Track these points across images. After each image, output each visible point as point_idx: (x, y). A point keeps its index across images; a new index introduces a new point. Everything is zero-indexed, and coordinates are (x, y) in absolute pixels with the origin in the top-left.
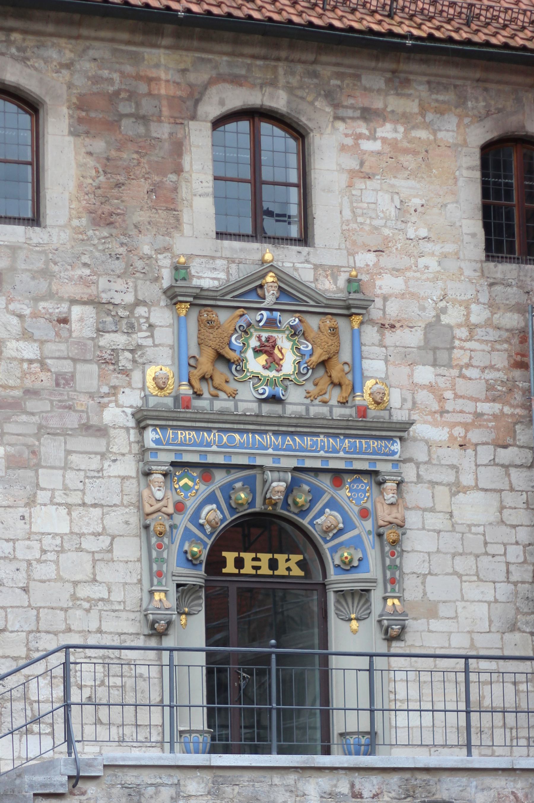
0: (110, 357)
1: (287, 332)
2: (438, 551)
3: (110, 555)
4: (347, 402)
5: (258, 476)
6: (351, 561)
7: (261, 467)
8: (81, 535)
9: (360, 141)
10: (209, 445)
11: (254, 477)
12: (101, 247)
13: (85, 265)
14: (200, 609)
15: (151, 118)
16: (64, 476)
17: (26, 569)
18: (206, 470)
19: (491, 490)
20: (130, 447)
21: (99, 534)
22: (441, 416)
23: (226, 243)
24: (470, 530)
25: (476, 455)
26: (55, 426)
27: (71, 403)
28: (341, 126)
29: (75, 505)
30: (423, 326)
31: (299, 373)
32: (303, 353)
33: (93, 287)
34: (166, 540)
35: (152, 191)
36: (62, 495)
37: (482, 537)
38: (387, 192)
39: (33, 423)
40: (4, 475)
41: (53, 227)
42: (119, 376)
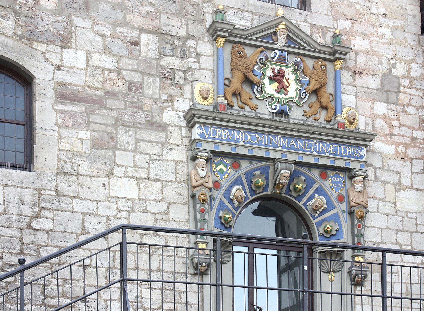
0: (168, 74)
1: (292, 68)
2: (387, 228)
3: (167, 216)
4: (331, 121)
5: (271, 166)
6: (331, 231)
7: (273, 159)
8: (147, 201)
11: (268, 167)
14: (229, 259)
16: (134, 157)
17: (105, 222)
18: (236, 158)
20: (182, 140)
21: (160, 201)
22: (391, 138)
24: (407, 216)
26: (128, 120)
27: (140, 104)
29: (142, 179)
30: (381, 75)
31: (300, 98)
32: (302, 83)
33: (157, 21)
34: (207, 206)
36: (133, 170)
37: (414, 220)
39: (112, 116)
40: (90, 152)
42: (175, 88)
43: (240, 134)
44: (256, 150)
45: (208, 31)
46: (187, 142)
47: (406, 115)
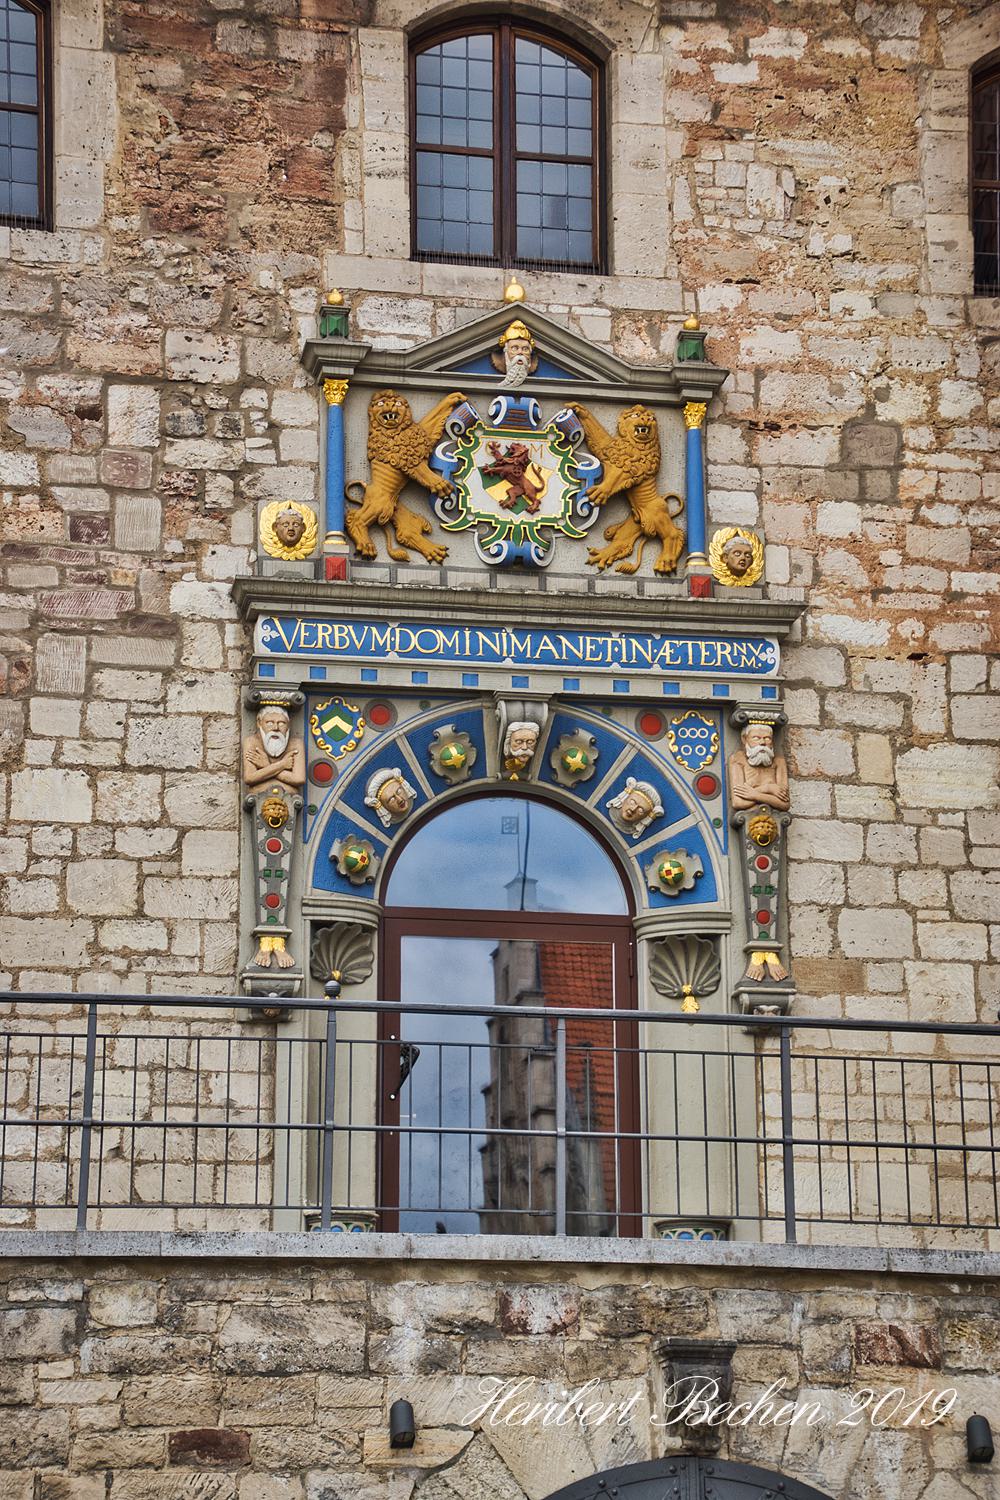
0: (186, 485)
2: (865, 861)
4: (674, 571)
6: (679, 879)
8: (115, 827)
9: (713, 66)
10: (381, 651)
11: (478, 715)
12: (170, 273)
13: (138, 306)
14: (367, 972)
15: (279, 21)
16: (83, 713)
18: (379, 701)
19: (980, 742)
20: (225, 657)
21: (154, 825)
22: (874, 599)
23: (431, 268)
25: (948, 674)
27: (102, 572)
28: (674, 36)
29: (106, 769)
31: (574, 517)
34: (287, 835)
35: (279, 165)
37: (961, 835)
38: (769, 164)
41: (70, 230)
42: (206, 521)
43: (388, 633)
44: (437, 673)
45: (302, 362)
46: (239, 660)
47: (924, 530)
